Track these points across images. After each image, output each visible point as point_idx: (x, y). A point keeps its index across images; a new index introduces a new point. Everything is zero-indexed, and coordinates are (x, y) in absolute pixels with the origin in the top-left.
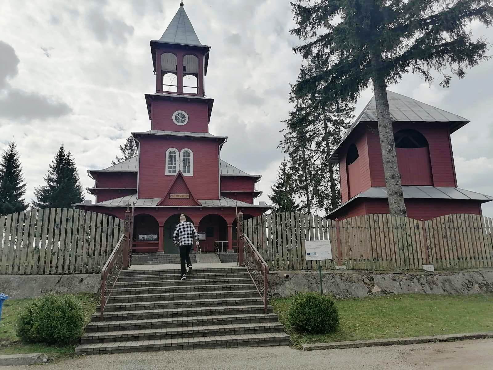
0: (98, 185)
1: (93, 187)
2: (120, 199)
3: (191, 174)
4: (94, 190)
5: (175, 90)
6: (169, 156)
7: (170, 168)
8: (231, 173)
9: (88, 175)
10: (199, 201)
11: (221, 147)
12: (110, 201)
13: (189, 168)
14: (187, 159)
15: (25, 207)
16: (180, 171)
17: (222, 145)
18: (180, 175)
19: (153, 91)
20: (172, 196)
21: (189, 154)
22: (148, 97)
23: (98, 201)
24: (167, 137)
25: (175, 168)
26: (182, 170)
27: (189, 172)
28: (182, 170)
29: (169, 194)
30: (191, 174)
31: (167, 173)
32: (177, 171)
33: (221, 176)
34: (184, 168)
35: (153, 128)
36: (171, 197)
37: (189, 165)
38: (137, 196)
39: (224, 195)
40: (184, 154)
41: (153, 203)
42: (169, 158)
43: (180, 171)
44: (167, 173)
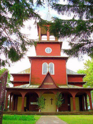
0: (14, 80)
2: (22, 86)
3: (54, 74)
8: (71, 73)
11: (67, 61)
12: (18, 86)
15: (76, 96)
17: (67, 61)
20: (45, 84)
23: (14, 86)
24: (43, 58)
26: (49, 71)
27: (52, 73)
29: (44, 82)
30: (54, 74)
31: (43, 74)
32: (47, 72)
33: (67, 74)
34: (50, 71)
35: (37, 55)
38: (30, 84)
39: (69, 83)
41: (36, 87)
44: (43, 74)
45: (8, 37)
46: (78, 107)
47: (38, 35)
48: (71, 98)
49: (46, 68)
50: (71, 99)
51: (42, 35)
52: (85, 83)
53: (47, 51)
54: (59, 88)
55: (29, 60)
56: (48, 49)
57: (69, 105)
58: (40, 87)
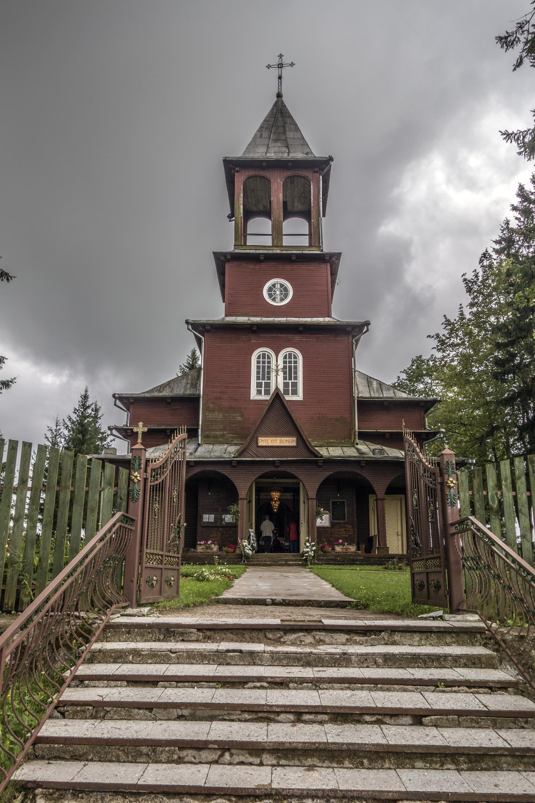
1: (124, 426)
3: (300, 397)
4: (126, 430)
5: (268, 241)
6: (258, 362)
7: (259, 385)
9: (115, 405)
10: (316, 448)
11: (357, 341)
13: (295, 385)
14: (290, 367)
16: (277, 388)
18: (277, 396)
19: (230, 247)
21: (295, 357)
22: (217, 255)
25: (268, 385)
26: (281, 387)
27: (295, 392)
28: (281, 387)
30: (300, 397)
32: (273, 389)
34: (286, 385)
36: (261, 444)
37: (296, 378)
40: (285, 357)
42: (258, 367)
43: (277, 388)
44: (254, 395)
45: (486, 628)
46: (400, 537)
47: (232, 216)
48: (372, 499)
49: (269, 373)
50: (226, 266)
51: (248, 214)
52: (435, 434)
53: (270, 296)
54: (322, 457)
55: (196, 336)
56: (274, 285)
57: (485, 493)
58: (241, 453)
